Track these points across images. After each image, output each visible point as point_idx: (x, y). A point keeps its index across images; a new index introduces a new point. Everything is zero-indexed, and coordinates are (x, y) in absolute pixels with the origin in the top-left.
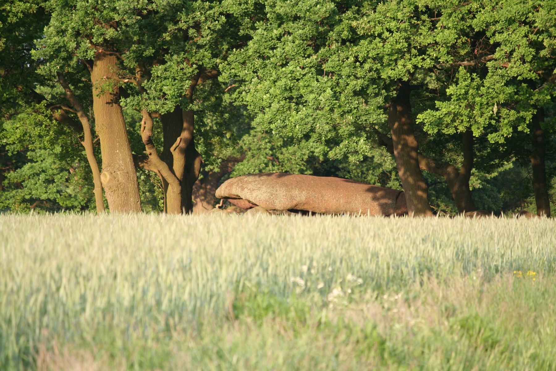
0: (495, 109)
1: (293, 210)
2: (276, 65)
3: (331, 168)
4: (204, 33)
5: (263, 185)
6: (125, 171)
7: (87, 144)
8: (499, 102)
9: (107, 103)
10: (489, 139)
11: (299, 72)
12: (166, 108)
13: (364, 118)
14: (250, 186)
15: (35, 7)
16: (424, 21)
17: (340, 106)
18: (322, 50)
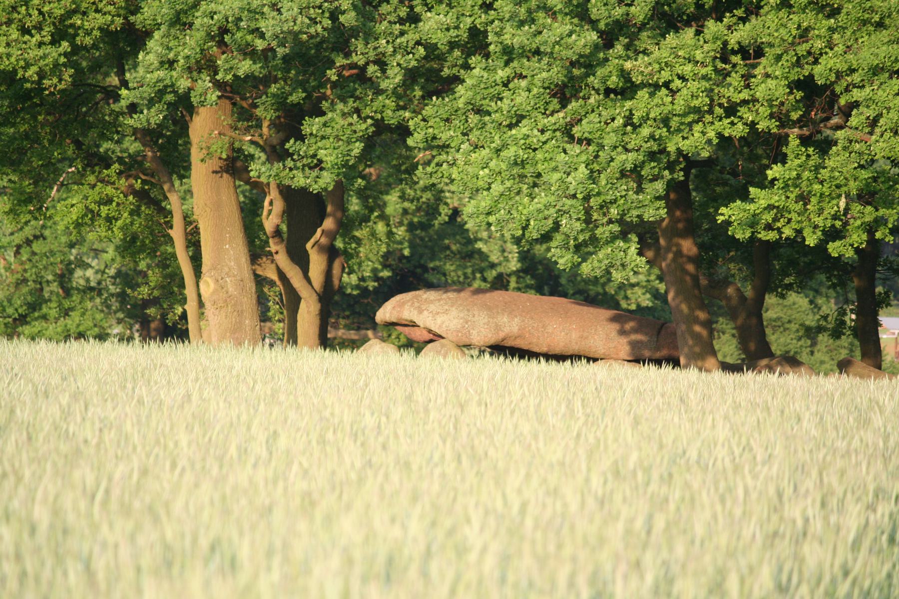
0: (842, 203)
1: (500, 349)
2: (500, 124)
3: (416, 267)
5: (452, 306)
6: (239, 278)
7: (177, 233)
8: (849, 192)
9: (214, 172)
10: (830, 250)
11: (536, 138)
12: (322, 183)
13: (635, 213)
14: (432, 307)
15: (119, 21)
16: (734, 66)
18: (573, 105)
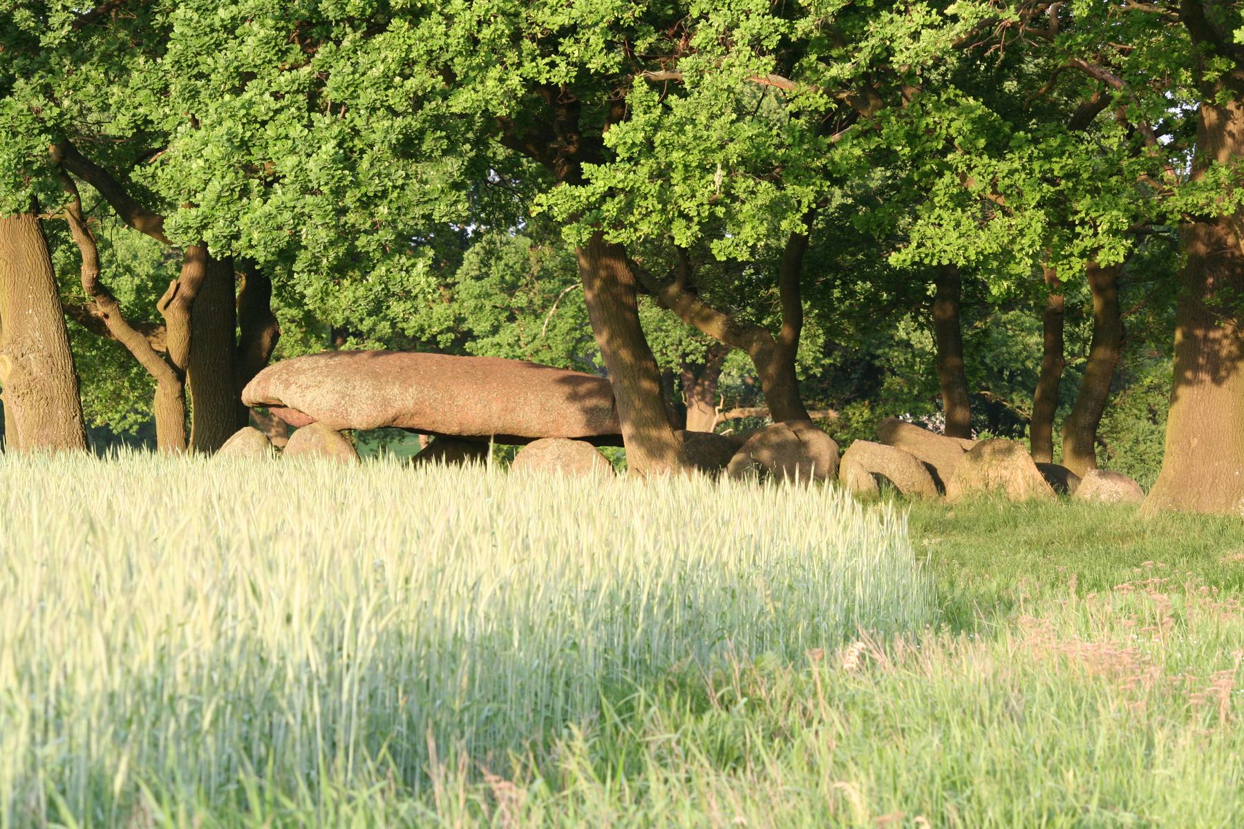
4: (54, 21)
5: (327, 376)
10: (714, 252)
13: (418, 211)
14: (303, 379)
17: (357, 184)
18: (323, 51)
